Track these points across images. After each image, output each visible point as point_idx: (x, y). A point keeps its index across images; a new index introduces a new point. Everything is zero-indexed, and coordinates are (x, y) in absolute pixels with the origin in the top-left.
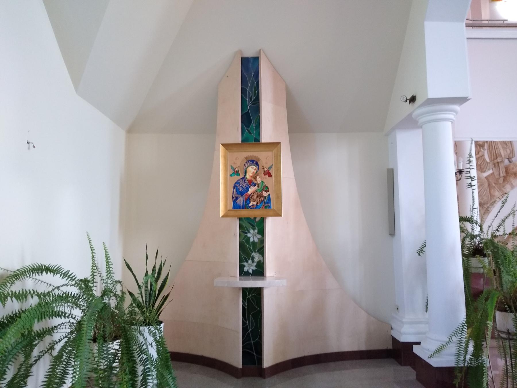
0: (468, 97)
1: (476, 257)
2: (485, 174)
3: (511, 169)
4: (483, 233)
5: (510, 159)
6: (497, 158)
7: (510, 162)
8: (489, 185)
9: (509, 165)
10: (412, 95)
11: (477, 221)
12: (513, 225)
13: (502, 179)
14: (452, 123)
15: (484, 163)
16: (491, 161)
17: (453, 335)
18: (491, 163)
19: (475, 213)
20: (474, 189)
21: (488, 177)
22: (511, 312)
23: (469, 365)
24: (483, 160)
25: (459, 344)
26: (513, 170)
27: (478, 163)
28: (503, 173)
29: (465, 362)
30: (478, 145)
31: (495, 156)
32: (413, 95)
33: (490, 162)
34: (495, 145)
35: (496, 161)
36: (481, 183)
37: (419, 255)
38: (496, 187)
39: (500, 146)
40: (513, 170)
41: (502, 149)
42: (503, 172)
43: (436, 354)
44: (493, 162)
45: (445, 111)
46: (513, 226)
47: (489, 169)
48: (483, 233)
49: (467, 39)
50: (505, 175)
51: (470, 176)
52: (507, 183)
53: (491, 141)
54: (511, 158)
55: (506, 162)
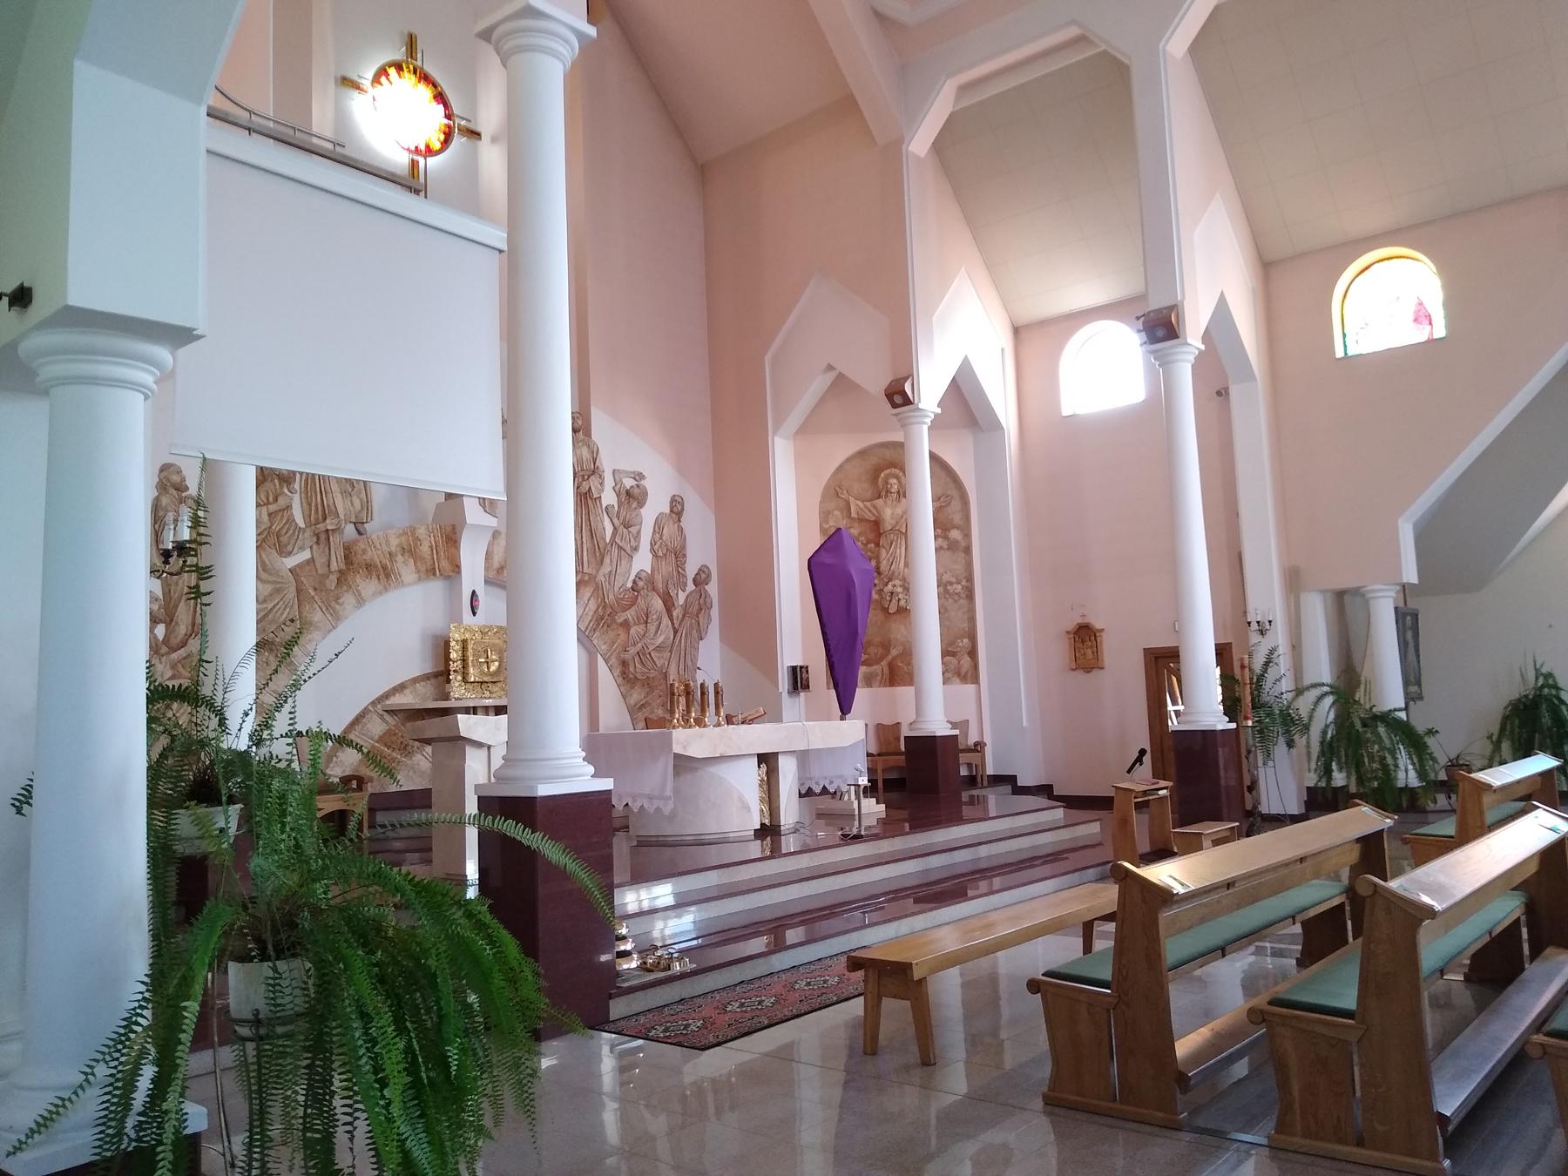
0: (195, 330)
1: (187, 808)
2: (291, 562)
3: (360, 552)
4: (228, 733)
5: (359, 526)
6: (325, 519)
7: (360, 533)
8: (299, 591)
9: (355, 542)
10: (18, 284)
11: (214, 697)
12: (293, 710)
13: (334, 578)
14: (146, 397)
15: (288, 529)
16: (309, 524)
17: (97, 1061)
18: (308, 530)
19: (205, 675)
20: (206, 605)
21: (298, 570)
22: (264, 957)
23: (134, 1144)
24: (288, 520)
25: (111, 1084)
26: (364, 557)
27: (274, 527)
28: (337, 562)
29: (121, 1140)
30: (275, 476)
31: (320, 512)
32: (22, 284)
33: (306, 527)
34: (322, 481)
35: (321, 527)
36: (278, 586)
37: (19, 812)
38: (316, 598)
39: (335, 487)
40: (364, 557)
41: (339, 495)
42: (339, 560)
43: (36, 1135)
44: (313, 527)
45: (131, 358)
46: (290, 713)
47: (302, 548)
48: (228, 733)
49: (207, 151)
50: (343, 566)
51: (196, 565)
52: (347, 591)
53: (313, 475)
54: (363, 523)
55: (350, 530)
